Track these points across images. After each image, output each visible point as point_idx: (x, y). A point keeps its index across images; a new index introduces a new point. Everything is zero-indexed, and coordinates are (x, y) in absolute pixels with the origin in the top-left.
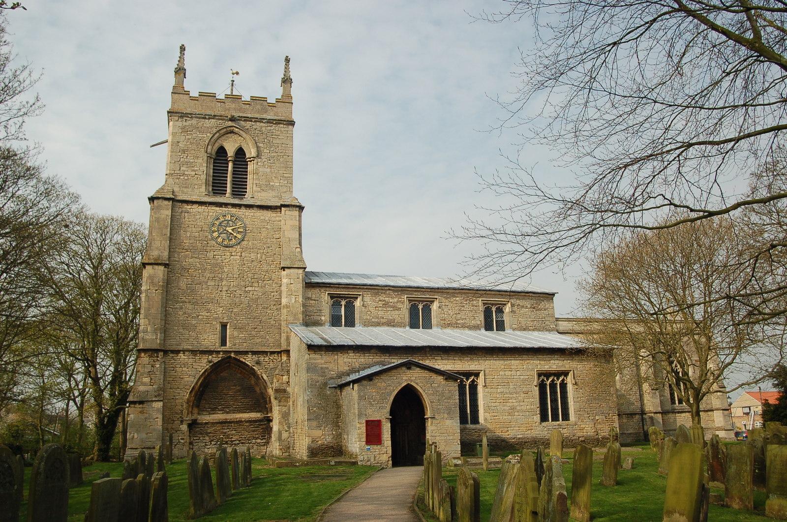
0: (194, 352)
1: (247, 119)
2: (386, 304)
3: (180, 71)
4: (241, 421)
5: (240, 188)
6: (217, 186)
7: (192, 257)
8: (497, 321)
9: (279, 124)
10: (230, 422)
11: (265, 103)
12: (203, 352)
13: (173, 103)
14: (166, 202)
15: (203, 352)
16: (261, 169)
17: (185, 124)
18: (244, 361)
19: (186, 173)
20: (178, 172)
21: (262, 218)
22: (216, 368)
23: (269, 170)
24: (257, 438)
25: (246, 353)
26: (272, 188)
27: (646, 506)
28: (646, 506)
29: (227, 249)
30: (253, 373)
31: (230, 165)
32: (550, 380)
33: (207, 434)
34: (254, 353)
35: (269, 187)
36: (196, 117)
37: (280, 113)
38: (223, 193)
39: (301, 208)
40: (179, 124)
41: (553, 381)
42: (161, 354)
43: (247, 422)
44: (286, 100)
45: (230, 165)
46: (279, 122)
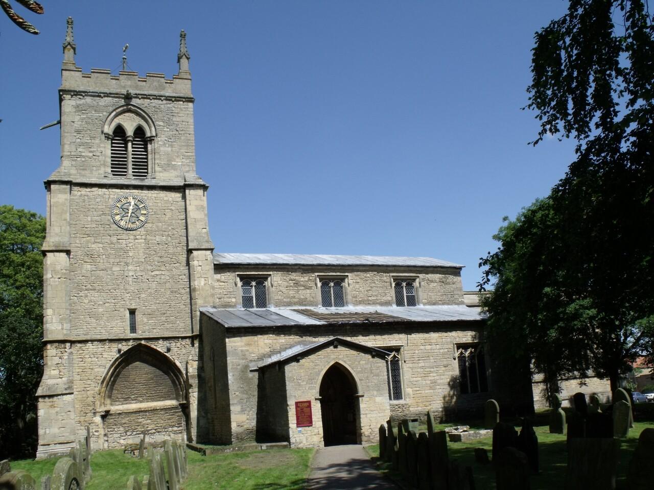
2: (297, 284)
5: (142, 167)
6: (118, 166)
12: (111, 341)
15: (111, 341)
16: (162, 149)
19: (83, 154)
21: (165, 199)
23: (170, 149)
24: (173, 426)
26: (174, 168)
35: (168, 166)
43: (162, 410)
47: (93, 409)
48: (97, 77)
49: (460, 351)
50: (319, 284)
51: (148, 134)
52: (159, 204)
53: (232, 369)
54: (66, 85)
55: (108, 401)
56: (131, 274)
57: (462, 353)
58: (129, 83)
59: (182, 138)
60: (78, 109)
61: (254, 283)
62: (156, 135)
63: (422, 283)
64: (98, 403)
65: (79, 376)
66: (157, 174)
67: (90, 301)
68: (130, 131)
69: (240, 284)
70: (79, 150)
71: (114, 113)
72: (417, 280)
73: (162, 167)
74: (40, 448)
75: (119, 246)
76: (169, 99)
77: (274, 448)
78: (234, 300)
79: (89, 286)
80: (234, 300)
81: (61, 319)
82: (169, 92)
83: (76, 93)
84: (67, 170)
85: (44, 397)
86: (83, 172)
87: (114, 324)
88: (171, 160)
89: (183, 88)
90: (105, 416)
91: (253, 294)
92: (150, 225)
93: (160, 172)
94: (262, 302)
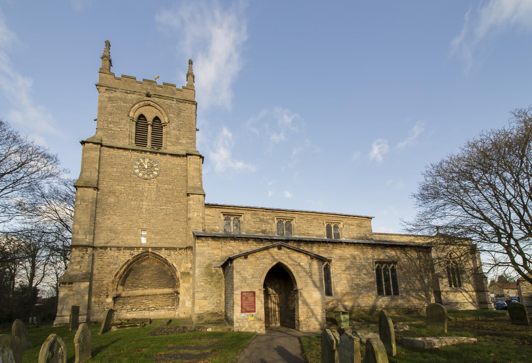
0: (119, 248)
1: (160, 96)
2: (262, 220)
3: (107, 59)
4: (157, 295)
5: (158, 142)
6: (140, 139)
7: (118, 185)
8: (334, 233)
9: (185, 103)
10: (148, 295)
11: (174, 88)
12: (126, 248)
13: (101, 79)
14: (95, 146)
15: (126, 248)
16: (172, 131)
17: (110, 95)
18: (159, 254)
19: (113, 129)
20: (107, 128)
21: (173, 162)
22: (138, 259)
23: (178, 132)
24: (168, 306)
25: (161, 248)
26: (180, 144)
27: (522, 333)
28: (522, 333)
29: (147, 181)
30: (166, 262)
31: (150, 128)
32: (383, 267)
33: (129, 304)
34: (167, 249)
35: (177, 143)
36: (120, 92)
37: (187, 95)
38: (145, 145)
39: (202, 157)
40: (107, 95)
41: (386, 267)
42: (90, 250)
43: (160, 295)
44: (190, 88)
45: (150, 128)
46: (185, 101)
47: (107, 293)
48: (126, 81)
49: (377, 265)
50: (276, 222)
51: (163, 122)
52: (169, 166)
53: (199, 265)
55: (120, 288)
56: (144, 207)
57: (378, 266)
58: (150, 87)
59: (187, 127)
61: (232, 218)
62: (169, 122)
63: (345, 226)
65: (98, 271)
66: (168, 147)
67: (112, 222)
68: (150, 119)
69: (223, 218)
70: (110, 126)
71: (137, 105)
72: (342, 223)
73: (172, 143)
75: (137, 189)
76: (179, 101)
77: (250, 242)
78: (218, 228)
79: (112, 212)
80: (218, 228)
81: (86, 232)
86: (113, 140)
87: (129, 237)
92: (161, 178)
93: (170, 146)
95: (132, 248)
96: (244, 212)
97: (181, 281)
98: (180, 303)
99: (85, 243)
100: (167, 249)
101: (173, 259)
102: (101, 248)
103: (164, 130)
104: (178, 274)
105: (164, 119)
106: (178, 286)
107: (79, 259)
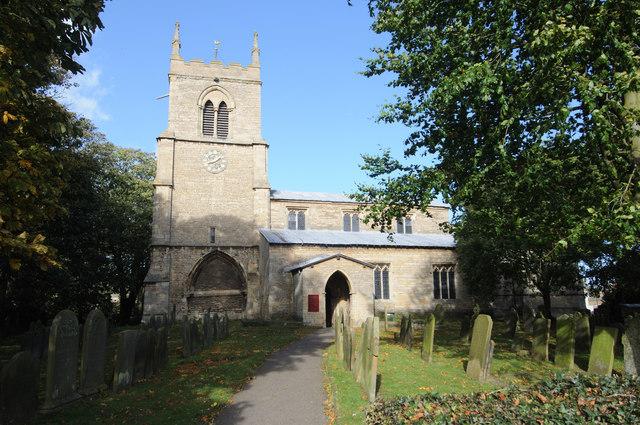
5: (223, 131)
6: (207, 129)
12: (197, 247)
15: (198, 247)
22: (208, 258)
25: (228, 248)
30: (232, 261)
34: (234, 248)
54: (173, 70)
55: (193, 288)
60: (181, 88)
61: (297, 212)
64: (185, 289)
74: (144, 317)
82: (243, 77)
83: (180, 77)
84: (173, 129)
85: (149, 283)
88: (242, 125)
89: (255, 74)
90: (190, 298)
91: (297, 220)
94: (302, 227)
95: (202, 247)
96: (310, 205)
97: (248, 283)
98: (248, 305)
99: (163, 243)
100: (234, 248)
101: (241, 259)
102: (176, 247)
103: (230, 115)
104: (245, 275)
105: (230, 105)
106: (246, 287)
107: (159, 259)
